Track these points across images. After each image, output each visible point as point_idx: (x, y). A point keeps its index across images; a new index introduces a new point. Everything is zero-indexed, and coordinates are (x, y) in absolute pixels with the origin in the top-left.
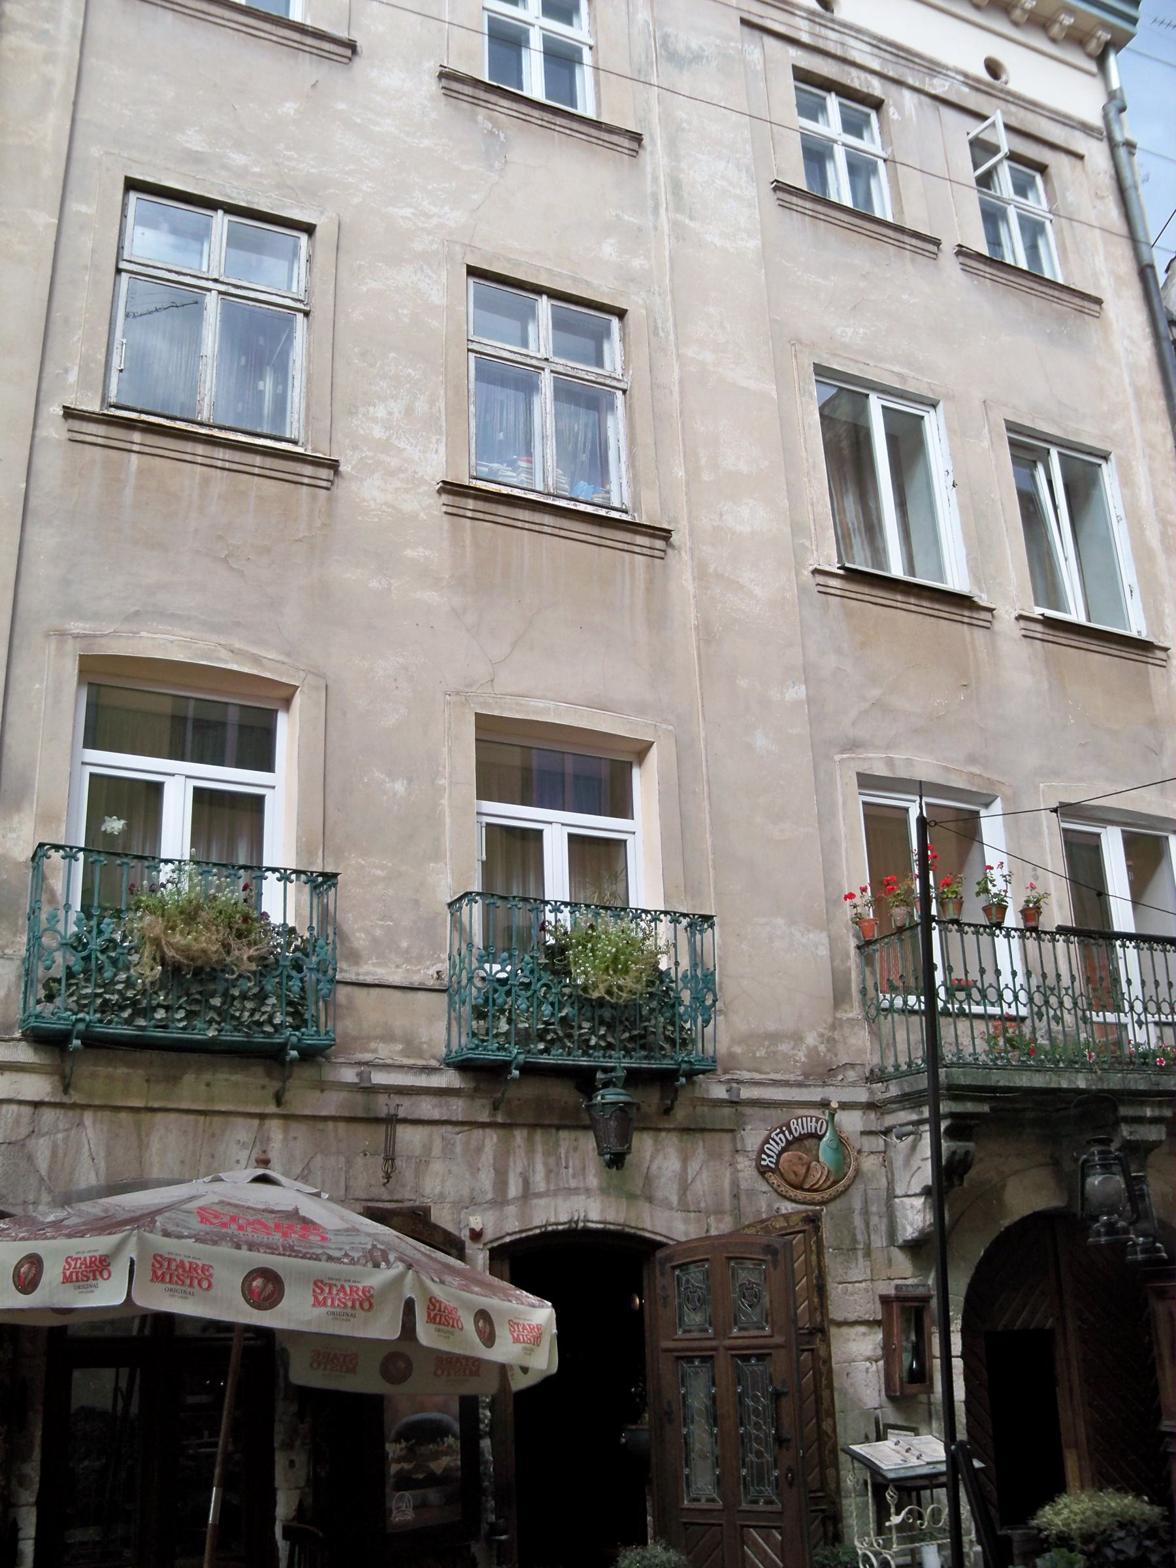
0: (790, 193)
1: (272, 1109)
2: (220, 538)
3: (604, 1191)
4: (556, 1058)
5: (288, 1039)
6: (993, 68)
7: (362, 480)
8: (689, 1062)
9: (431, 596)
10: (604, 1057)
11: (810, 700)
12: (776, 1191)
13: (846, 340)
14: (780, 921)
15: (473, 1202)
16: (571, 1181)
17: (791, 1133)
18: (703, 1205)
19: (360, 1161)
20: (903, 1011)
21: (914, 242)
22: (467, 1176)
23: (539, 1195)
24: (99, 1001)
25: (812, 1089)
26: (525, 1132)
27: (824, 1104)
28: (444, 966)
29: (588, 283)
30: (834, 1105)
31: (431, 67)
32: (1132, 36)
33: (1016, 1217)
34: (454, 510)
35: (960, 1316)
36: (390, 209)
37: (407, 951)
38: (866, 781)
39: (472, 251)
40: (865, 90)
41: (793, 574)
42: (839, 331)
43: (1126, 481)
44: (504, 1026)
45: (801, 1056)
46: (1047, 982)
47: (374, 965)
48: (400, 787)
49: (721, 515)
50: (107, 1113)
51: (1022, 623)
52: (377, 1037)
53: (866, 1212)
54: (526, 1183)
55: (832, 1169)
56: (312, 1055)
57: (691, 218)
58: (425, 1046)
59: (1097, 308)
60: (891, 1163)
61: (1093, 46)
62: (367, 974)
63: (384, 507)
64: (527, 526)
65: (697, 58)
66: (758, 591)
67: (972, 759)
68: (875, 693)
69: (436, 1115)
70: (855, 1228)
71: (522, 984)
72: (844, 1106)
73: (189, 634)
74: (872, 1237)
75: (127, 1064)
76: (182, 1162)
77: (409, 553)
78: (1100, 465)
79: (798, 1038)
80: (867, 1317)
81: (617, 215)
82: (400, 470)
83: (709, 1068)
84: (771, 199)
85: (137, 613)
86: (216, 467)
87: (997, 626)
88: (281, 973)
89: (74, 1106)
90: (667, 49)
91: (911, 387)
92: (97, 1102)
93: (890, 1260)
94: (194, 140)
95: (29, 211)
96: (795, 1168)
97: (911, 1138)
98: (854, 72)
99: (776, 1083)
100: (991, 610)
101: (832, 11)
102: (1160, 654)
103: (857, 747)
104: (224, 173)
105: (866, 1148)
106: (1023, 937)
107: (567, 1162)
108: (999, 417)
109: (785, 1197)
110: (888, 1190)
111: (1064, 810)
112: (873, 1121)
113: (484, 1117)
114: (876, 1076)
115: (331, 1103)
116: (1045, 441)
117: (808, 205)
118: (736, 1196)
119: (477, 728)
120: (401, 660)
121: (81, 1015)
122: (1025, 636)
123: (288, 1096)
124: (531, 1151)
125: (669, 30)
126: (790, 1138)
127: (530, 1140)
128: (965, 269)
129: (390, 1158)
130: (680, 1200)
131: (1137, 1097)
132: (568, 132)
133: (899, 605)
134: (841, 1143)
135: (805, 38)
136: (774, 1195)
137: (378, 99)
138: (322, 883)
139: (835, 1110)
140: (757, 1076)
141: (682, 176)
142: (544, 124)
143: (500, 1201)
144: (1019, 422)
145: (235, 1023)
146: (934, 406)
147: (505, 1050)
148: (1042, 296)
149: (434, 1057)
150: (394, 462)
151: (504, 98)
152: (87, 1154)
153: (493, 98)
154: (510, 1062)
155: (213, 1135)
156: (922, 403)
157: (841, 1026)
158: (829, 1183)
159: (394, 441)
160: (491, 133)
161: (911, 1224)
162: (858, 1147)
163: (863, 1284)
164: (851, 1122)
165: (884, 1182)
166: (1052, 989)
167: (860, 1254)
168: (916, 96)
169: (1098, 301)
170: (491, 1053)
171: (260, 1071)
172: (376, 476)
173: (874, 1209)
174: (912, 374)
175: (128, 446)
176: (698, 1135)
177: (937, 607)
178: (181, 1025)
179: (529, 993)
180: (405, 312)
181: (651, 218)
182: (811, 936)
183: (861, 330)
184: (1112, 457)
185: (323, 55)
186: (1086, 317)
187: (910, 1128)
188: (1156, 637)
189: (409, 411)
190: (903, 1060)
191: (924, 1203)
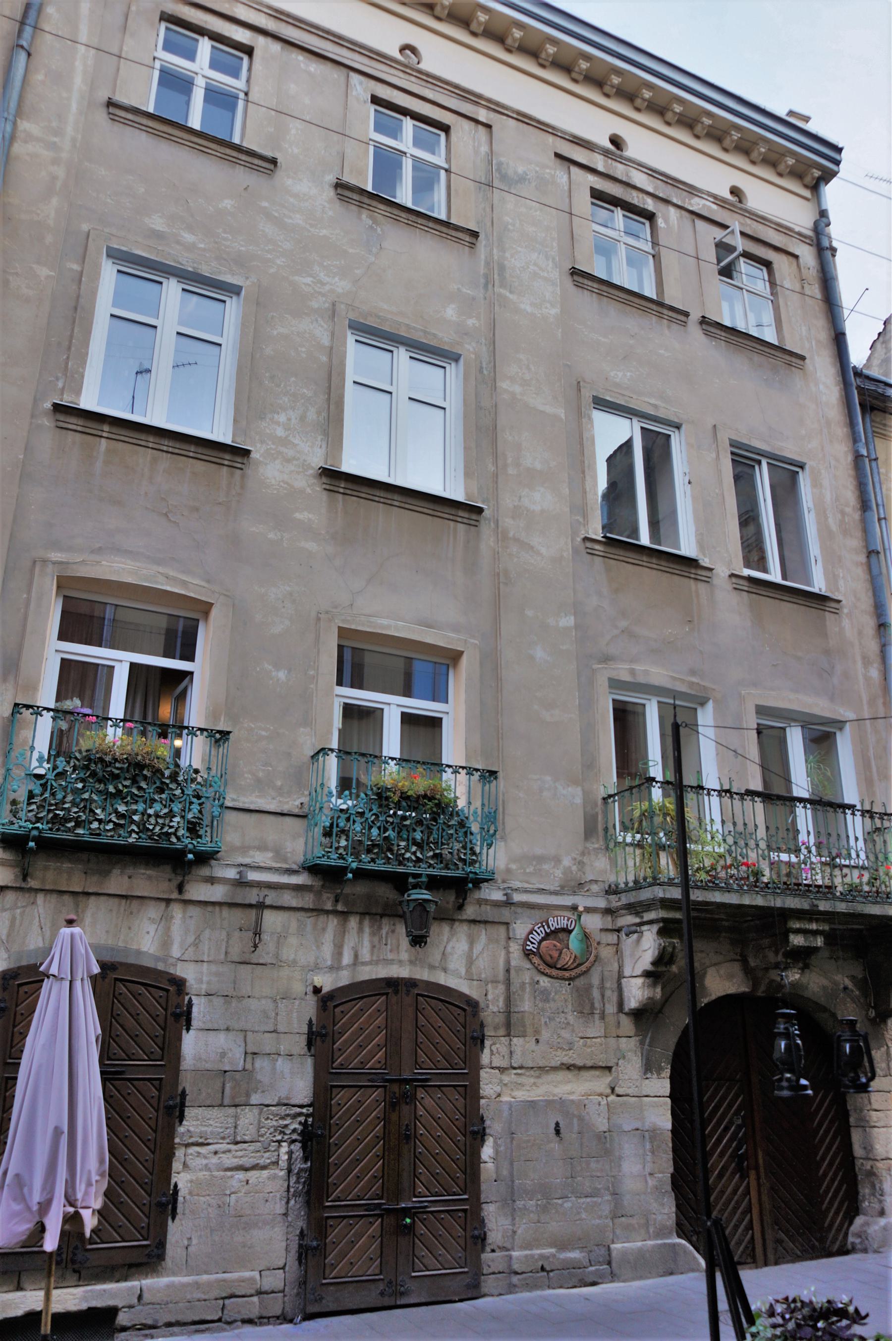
0: (583, 277)
1: (175, 895)
2: (163, 499)
3: (411, 962)
4: (379, 866)
5: (186, 846)
6: (735, 191)
7: (266, 464)
8: (475, 873)
9: (311, 546)
10: (414, 866)
11: (577, 626)
12: (537, 968)
13: (618, 380)
14: (548, 778)
15: (316, 968)
16: (389, 953)
17: (549, 927)
18: (483, 976)
19: (237, 934)
20: (631, 844)
21: (671, 314)
22: (314, 948)
23: (364, 964)
24: (51, 815)
25: (566, 897)
26: (358, 918)
27: (574, 908)
28: (306, 800)
29: (435, 335)
30: (581, 909)
31: (331, 178)
32: (834, 174)
33: (713, 997)
34: (332, 488)
35: (669, 1066)
36: (296, 278)
37: (280, 788)
38: (615, 684)
39: (353, 310)
40: (642, 206)
41: (569, 541)
42: (612, 374)
43: (816, 483)
44: (343, 843)
45: (558, 873)
46: (737, 828)
47: (257, 797)
48: (282, 675)
49: (520, 497)
50: (55, 896)
51: (734, 580)
52: (254, 847)
53: (602, 988)
54: (356, 956)
55: (578, 955)
56: (205, 858)
57: (511, 292)
58: (289, 855)
59: (801, 362)
60: (622, 953)
61: (808, 180)
62: (252, 803)
63: (282, 484)
64: (382, 500)
65: (522, 179)
66: (543, 550)
67: (693, 672)
68: (623, 624)
69: (294, 903)
70: (593, 999)
71: (358, 813)
72: (588, 910)
73: (138, 564)
74: (607, 1006)
75: (70, 861)
76: (107, 932)
77: (298, 515)
78: (798, 472)
79: (557, 860)
80: (601, 1064)
81: (458, 289)
82: (294, 458)
83: (488, 879)
84: (568, 282)
85: (100, 549)
86: (163, 451)
87: (716, 581)
88: (185, 800)
89: (30, 890)
90: (500, 173)
91: (661, 414)
92: (47, 888)
93: (619, 1023)
94: (157, 223)
95: (35, 266)
96: (551, 953)
97: (636, 935)
98: (635, 193)
99: (541, 891)
100: (711, 570)
101: (622, 151)
102: (833, 605)
103: (610, 660)
104: (178, 247)
105: (604, 941)
106: (720, 795)
107: (386, 940)
108: (724, 437)
109: (543, 973)
110: (619, 972)
111: (761, 711)
112: (608, 922)
113: (329, 906)
114: (612, 891)
115: (217, 893)
116: (758, 454)
117: (595, 285)
118: (508, 971)
119: (339, 637)
120: (288, 588)
121: (36, 825)
122: (735, 589)
123: (187, 887)
124: (361, 930)
125: (503, 159)
126: (548, 931)
127: (361, 923)
128: (707, 333)
129: (257, 933)
130: (467, 971)
131: (799, 914)
132: (426, 229)
133: (645, 564)
134: (586, 936)
135: (600, 168)
136: (534, 972)
137: (292, 200)
138: (220, 739)
139: (581, 912)
140: (526, 885)
141: (506, 262)
142: (410, 222)
143: (335, 968)
144: (739, 440)
145: (150, 833)
146: (678, 427)
147: (344, 859)
148: (761, 353)
149: (295, 863)
150: (290, 453)
151: (380, 203)
152: (37, 924)
153: (374, 203)
154: (346, 868)
155: (131, 913)
156: (670, 426)
157: (589, 853)
158: (575, 964)
159: (291, 438)
160: (371, 227)
161: (634, 997)
162: (598, 939)
163: (598, 1040)
164: (593, 922)
165: (616, 966)
166: (751, 834)
167: (597, 1017)
168: (678, 211)
169: (803, 358)
170: (333, 861)
171: (168, 868)
172: (277, 462)
173: (608, 985)
174: (663, 405)
175: (100, 433)
176: (482, 925)
177: (672, 566)
178: (109, 834)
179: (363, 820)
180: (303, 349)
181: (482, 291)
182: (570, 789)
183: (629, 374)
184: (807, 467)
185: (252, 168)
186: (793, 369)
187: (634, 928)
188: (833, 593)
189: (302, 418)
190: (631, 878)
191: (643, 983)
